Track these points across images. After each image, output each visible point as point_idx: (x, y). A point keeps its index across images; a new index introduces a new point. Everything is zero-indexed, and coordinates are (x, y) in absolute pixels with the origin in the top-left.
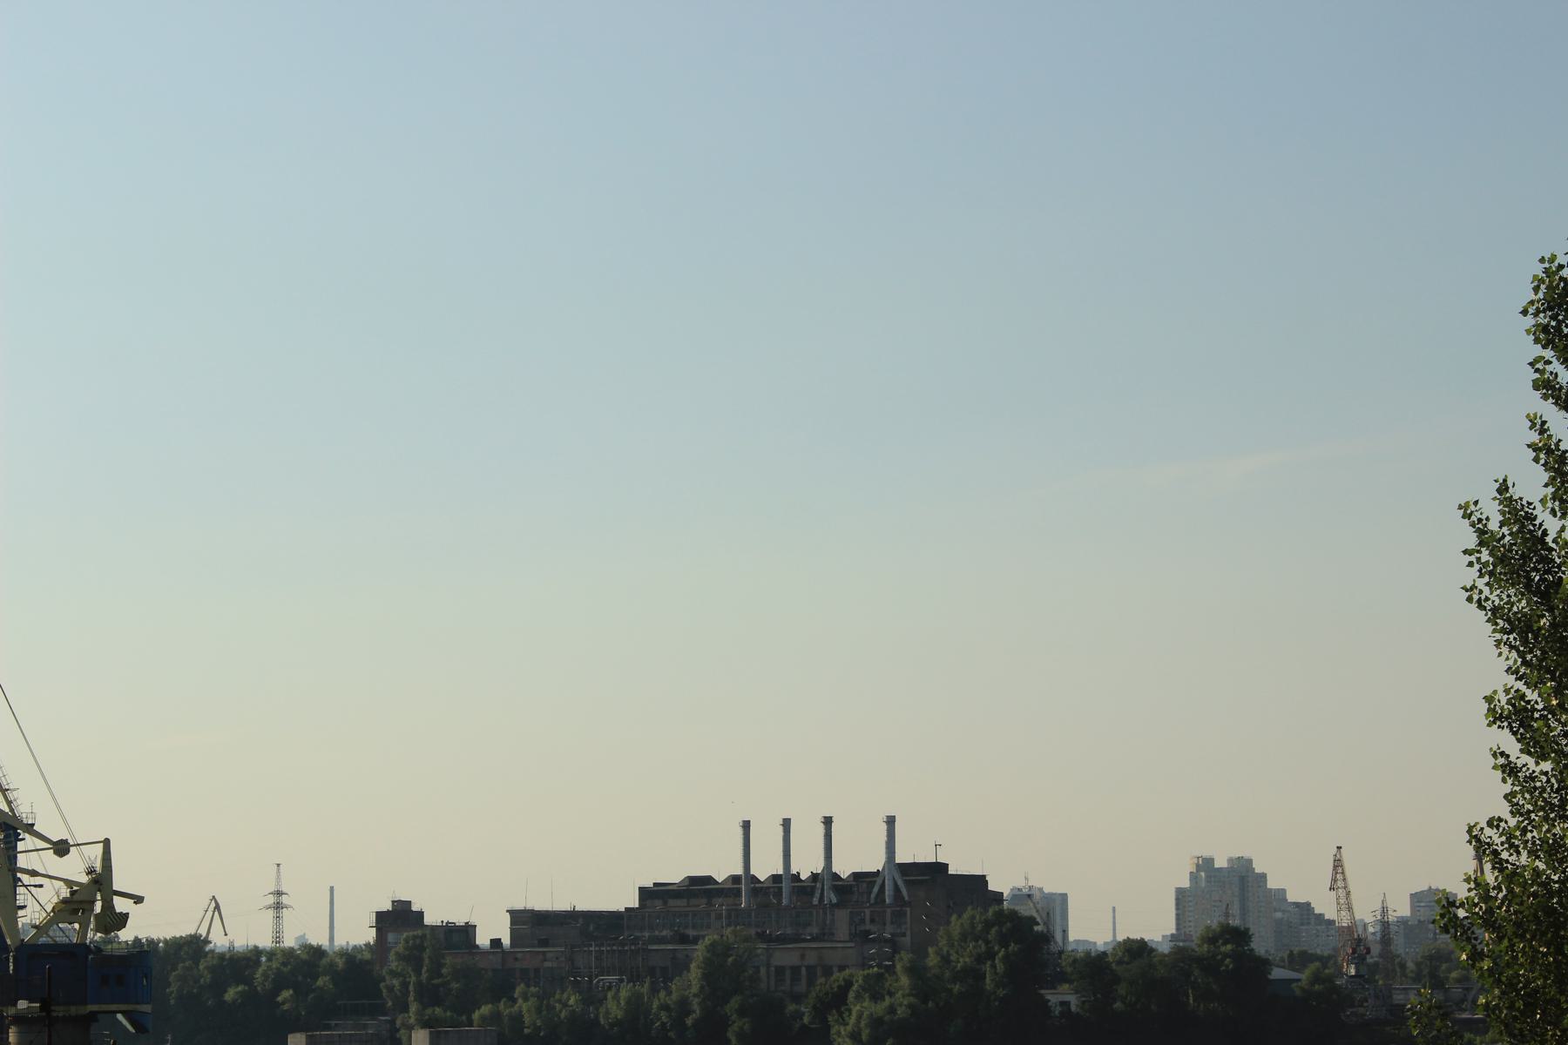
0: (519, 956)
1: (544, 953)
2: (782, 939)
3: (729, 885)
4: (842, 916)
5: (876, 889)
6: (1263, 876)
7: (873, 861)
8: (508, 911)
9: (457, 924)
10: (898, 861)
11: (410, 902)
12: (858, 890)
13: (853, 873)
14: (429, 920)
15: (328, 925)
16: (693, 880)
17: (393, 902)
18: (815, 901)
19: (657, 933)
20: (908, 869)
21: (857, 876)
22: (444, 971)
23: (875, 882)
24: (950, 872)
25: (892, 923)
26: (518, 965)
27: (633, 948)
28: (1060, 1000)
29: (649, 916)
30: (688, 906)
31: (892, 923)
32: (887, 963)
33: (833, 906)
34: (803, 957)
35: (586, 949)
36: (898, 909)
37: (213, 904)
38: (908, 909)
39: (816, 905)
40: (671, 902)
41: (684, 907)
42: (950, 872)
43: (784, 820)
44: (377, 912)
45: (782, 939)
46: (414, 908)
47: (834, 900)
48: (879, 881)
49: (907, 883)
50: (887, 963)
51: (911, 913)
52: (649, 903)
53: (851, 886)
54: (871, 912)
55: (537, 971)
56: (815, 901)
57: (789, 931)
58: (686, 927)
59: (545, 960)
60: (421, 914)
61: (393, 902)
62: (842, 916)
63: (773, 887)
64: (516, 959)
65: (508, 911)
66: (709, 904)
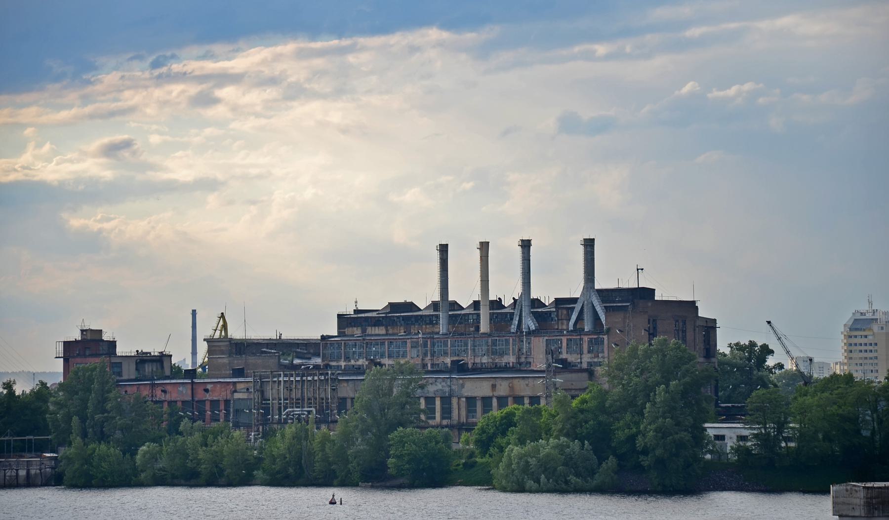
0: (209, 387)
1: (235, 383)
2: (477, 369)
3: (431, 312)
4: (539, 345)
5: (574, 317)
6: (113, 344)
7: (574, 289)
8: (205, 340)
9: (152, 354)
10: (598, 286)
11: (101, 331)
12: (557, 316)
13: (389, 303)
14: (121, 350)
15: (191, 351)
16: (393, 307)
17: (82, 331)
18: (513, 328)
19: (353, 362)
20: (606, 295)
21: (559, 302)
22: (109, 406)
23: (574, 308)
24: (656, 298)
25: (589, 352)
26: (208, 397)
27: (323, 378)
28: (716, 434)
29: (345, 343)
30: (387, 334)
31: (589, 352)
32: (217, 412)
33: (530, 333)
34: (494, 387)
35: (309, 378)
36: (595, 337)
37: (221, 323)
38: (605, 337)
39: (513, 333)
40: (370, 330)
41: (383, 335)
42: (656, 298)
43: (481, 243)
44: (64, 342)
45: (477, 369)
46: (106, 337)
47: (533, 327)
48: (578, 307)
49: (607, 309)
50: (217, 412)
51: (608, 338)
52: (348, 331)
53: (550, 312)
54: (567, 339)
55: (227, 402)
56: (513, 328)
57: (485, 360)
58: (382, 356)
59: (235, 391)
60: (113, 344)
61: (82, 331)
62: (539, 345)
63: (473, 314)
64: (207, 391)
65: (205, 340)
66: (407, 332)
